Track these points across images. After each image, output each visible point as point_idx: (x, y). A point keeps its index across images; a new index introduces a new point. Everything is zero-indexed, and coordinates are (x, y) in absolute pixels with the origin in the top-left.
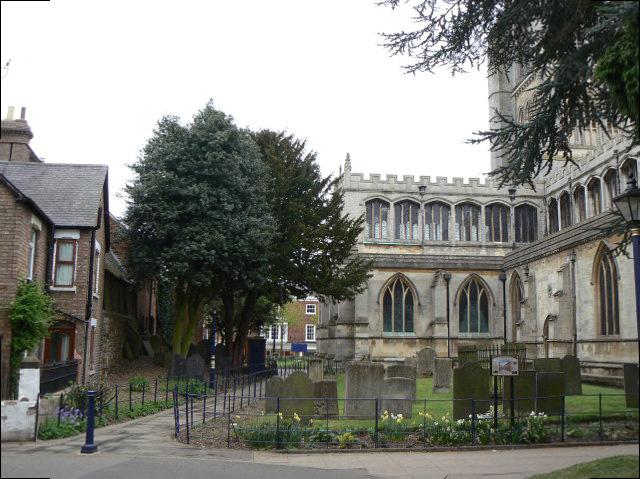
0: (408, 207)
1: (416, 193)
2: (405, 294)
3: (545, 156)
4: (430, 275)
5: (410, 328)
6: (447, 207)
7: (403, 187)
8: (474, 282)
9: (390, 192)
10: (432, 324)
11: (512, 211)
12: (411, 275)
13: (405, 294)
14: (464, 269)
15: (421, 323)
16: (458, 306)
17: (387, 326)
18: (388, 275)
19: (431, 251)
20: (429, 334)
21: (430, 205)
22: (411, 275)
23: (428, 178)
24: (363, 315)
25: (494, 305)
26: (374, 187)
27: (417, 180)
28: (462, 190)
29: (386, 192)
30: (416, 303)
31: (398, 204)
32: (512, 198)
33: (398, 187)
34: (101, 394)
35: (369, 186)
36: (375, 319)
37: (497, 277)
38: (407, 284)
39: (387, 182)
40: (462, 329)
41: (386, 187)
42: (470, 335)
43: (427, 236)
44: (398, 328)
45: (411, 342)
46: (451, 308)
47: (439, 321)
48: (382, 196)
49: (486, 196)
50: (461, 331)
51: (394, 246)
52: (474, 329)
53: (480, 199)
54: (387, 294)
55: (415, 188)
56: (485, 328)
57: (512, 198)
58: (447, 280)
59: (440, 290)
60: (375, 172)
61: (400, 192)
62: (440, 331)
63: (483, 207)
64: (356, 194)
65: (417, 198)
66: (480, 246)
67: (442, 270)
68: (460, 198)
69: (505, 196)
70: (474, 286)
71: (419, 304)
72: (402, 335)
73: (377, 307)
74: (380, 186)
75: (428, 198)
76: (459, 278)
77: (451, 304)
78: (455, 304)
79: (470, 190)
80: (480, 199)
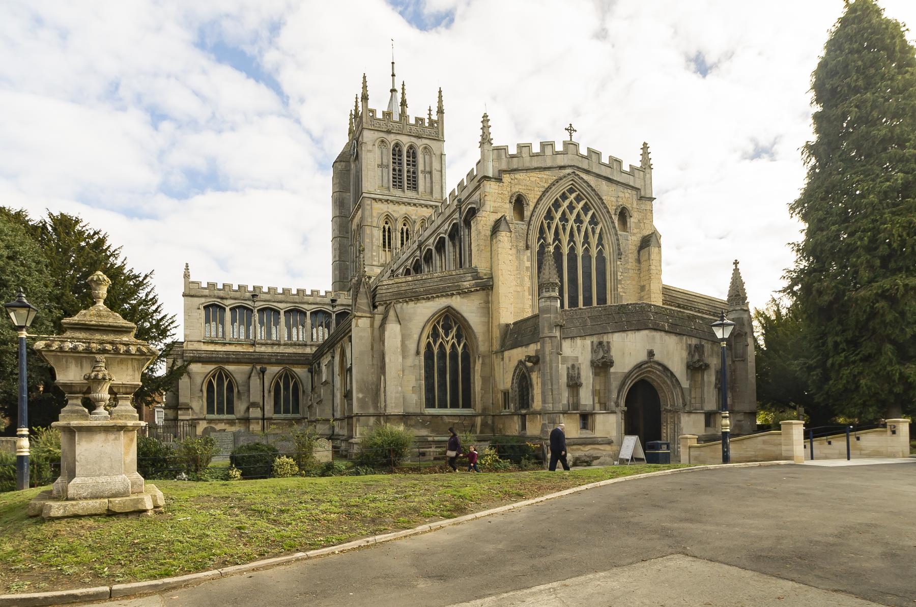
0: (243, 312)
1: (249, 300)
2: (226, 384)
3: (96, 237)
4: (247, 368)
5: (231, 411)
6: (277, 312)
7: (238, 295)
8: (286, 374)
9: (227, 299)
10: (248, 409)
11: (334, 316)
12: (230, 368)
13: (226, 384)
14: (277, 363)
15: (240, 407)
16: (272, 393)
17: (210, 410)
18: (210, 368)
19: (263, 349)
20: (246, 415)
21: (262, 311)
22: (230, 368)
23: (260, 288)
24: (187, 401)
25: (304, 392)
26: (212, 293)
27: (251, 289)
28: (290, 299)
29: (222, 298)
30: (236, 390)
31: (233, 310)
32: (333, 307)
33: (233, 294)
34: (593, 414)
35: (206, 292)
36: (199, 405)
37: (306, 370)
38: (228, 375)
39: (325, 297)
40: (277, 411)
41: (221, 294)
42: (282, 416)
43: (301, 337)
44: (220, 411)
45: (231, 423)
46: (266, 395)
47: (254, 405)
48: (218, 301)
49: (311, 304)
50: (275, 413)
51: (230, 344)
52: (286, 411)
53: (306, 306)
54: (210, 384)
55: (248, 295)
56: (296, 410)
57: (333, 307)
58: (263, 371)
59: (255, 382)
60: (212, 281)
61: (235, 299)
62: (255, 413)
63: (308, 313)
64: (195, 299)
65: (329, 309)
66: (306, 345)
67: (258, 362)
68: (314, 306)
69: (327, 304)
70: (287, 376)
71: (238, 391)
72: (225, 416)
73: (200, 394)
74: (318, 300)
75: (260, 305)
76: (273, 370)
77: (266, 392)
78: (270, 392)
79: (297, 299)
80: (306, 306)
